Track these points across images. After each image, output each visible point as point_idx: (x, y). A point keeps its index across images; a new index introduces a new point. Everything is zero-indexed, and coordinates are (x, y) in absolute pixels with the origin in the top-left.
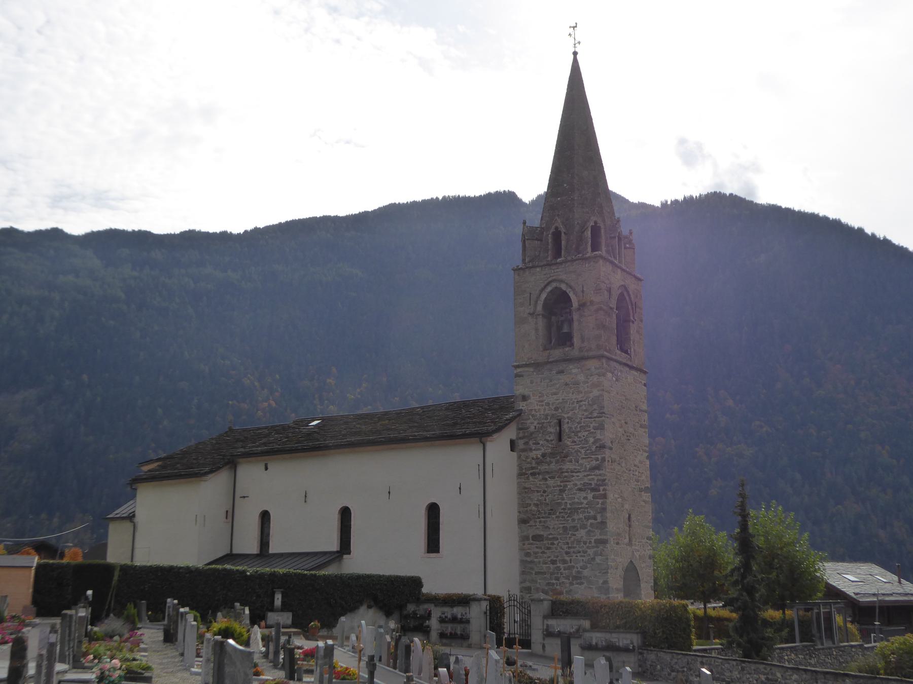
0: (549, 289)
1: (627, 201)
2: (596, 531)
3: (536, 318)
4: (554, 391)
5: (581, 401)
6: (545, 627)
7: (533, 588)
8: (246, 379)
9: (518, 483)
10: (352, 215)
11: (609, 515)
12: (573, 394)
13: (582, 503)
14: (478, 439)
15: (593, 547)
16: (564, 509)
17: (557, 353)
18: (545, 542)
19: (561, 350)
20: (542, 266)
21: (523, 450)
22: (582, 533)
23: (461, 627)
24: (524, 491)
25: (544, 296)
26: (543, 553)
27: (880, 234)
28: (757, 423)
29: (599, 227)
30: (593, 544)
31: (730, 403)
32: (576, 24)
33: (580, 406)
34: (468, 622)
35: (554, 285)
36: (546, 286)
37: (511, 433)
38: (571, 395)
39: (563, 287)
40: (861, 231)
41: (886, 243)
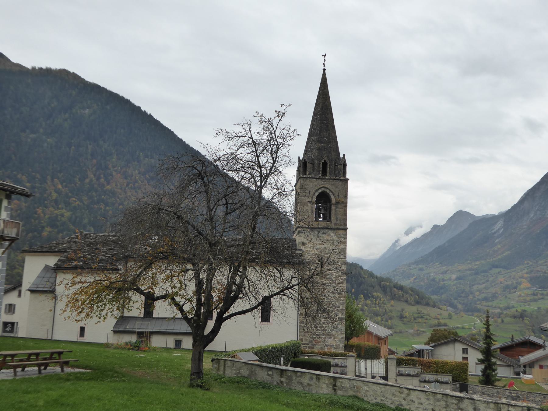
0: (320, 191)
1: (9, 60)
2: (339, 313)
3: (312, 204)
6: (397, 372)
7: (304, 339)
12: (330, 245)
19: (325, 223)
20: (316, 179)
23: (340, 369)
27: (148, 112)
28: (74, 199)
31: (60, 186)
32: (325, 54)
34: (346, 367)
35: (323, 189)
36: (317, 190)
38: (329, 246)
39: (328, 191)
40: (139, 108)
41: (150, 116)
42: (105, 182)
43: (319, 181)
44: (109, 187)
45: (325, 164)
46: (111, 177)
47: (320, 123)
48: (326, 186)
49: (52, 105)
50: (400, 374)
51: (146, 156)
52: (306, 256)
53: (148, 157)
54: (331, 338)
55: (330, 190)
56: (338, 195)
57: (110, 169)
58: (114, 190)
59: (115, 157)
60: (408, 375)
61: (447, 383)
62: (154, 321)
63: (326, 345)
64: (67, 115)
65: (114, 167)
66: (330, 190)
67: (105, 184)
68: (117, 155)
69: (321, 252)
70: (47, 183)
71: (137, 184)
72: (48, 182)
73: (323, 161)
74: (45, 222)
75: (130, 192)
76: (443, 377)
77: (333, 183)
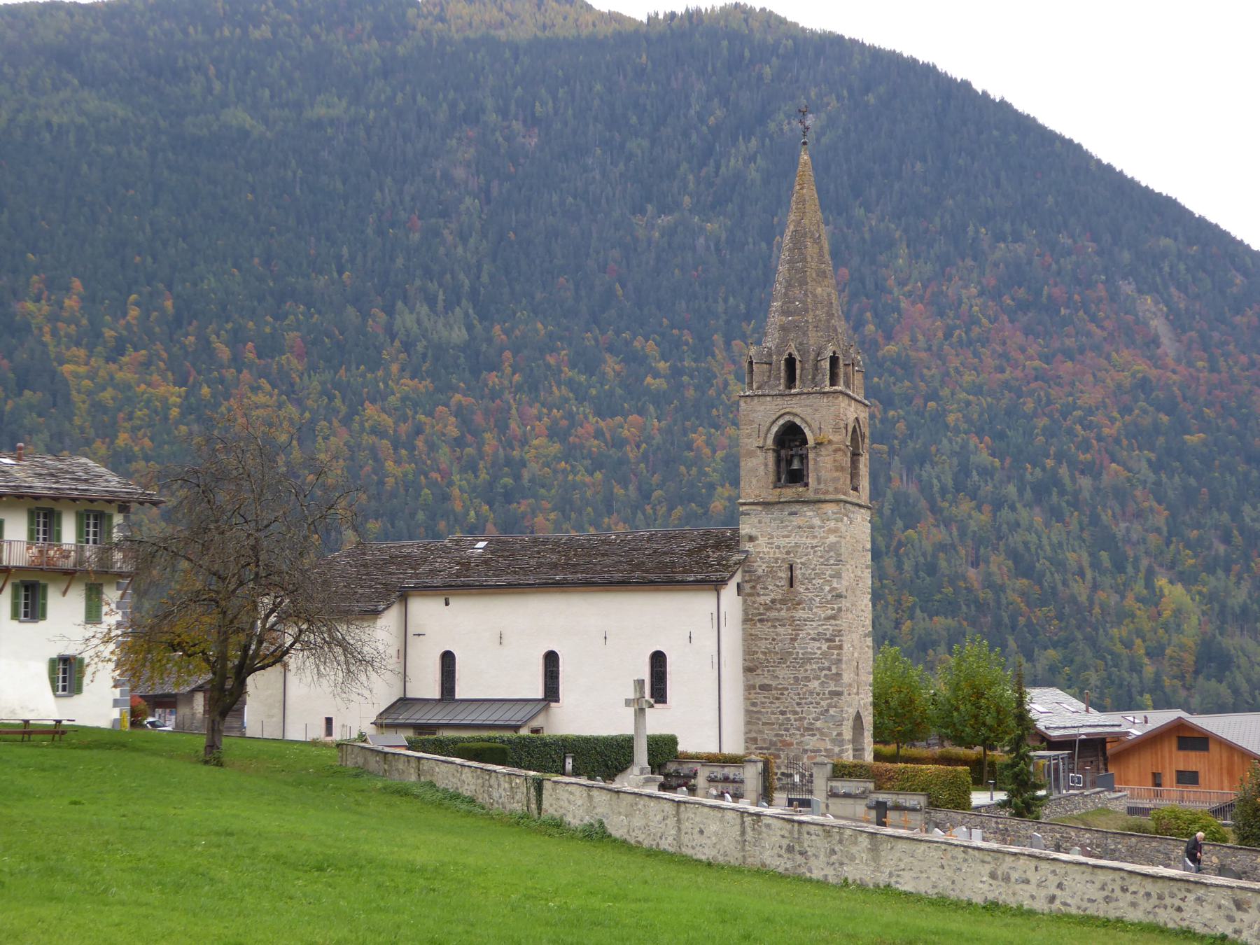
0: (781, 422)
13: (815, 653)
15: (827, 699)
17: (790, 492)
30: (827, 696)
34: (742, 782)
35: (787, 418)
36: (774, 422)
39: (798, 421)
42: (880, 332)
43: (779, 400)
44: (891, 348)
45: (791, 362)
46: (896, 315)
47: (789, 270)
48: (794, 411)
49: (712, 120)
50: (833, 794)
51: (999, 237)
52: (755, 564)
53: (1004, 241)
54: (815, 735)
55: (802, 419)
56: (820, 428)
57: (891, 292)
58: (907, 355)
59: (903, 250)
60: (847, 796)
61: (913, 810)
62: (455, 704)
63: (806, 751)
64: (754, 142)
65: (902, 283)
66: (802, 419)
67: (880, 340)
68: (908, 246)
69: (788, 553)
70: (713, 356)
71: (976, 330)
72: (717, 351)
73: (786, 356)
74: (715, 470)
75: (957, 355)
76: (908, 797)
77: (808, 402)
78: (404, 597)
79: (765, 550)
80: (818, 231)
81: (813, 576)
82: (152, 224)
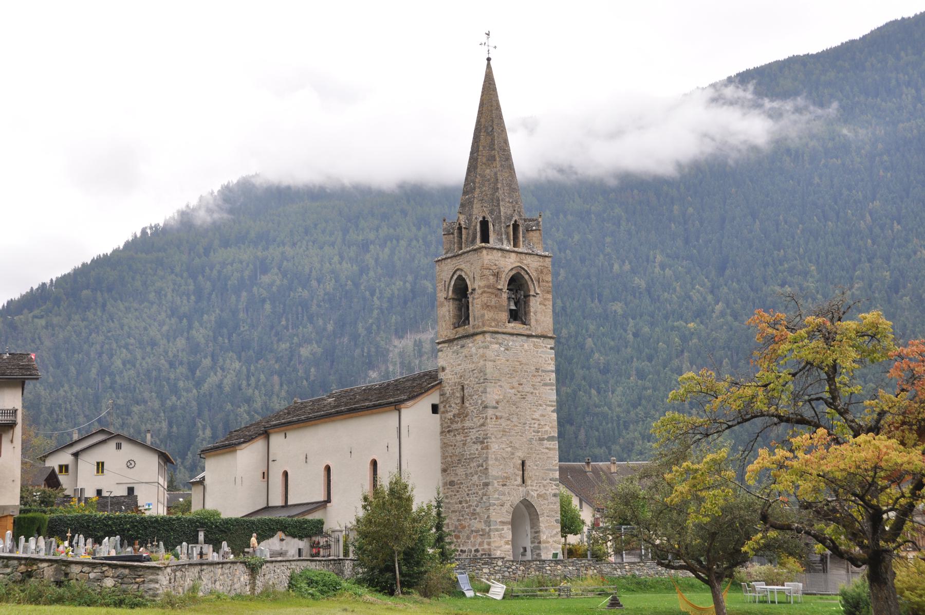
4: (459, 362)
5: (474, 370)
8: (694, 291)
9: (441, 439)
10: (831, 49)
11: (490, 462)
13: (475, 454)
14: (393, 407)
15: (482, 489)
16: (465, 459)
17: (461, 331)
18: (456, 487)
21: (443, 412)
22: (476, 477)
24: (444, 446)
25: (453, 283)
26: (455, 495)
29: (487, 221)
30: (482, 487)
33: (473, 374)
35: (458, 273)
36: (452, 278)
37: (433, 398)
56: (474, 277)
78: (266, 434)
79: (450, 377)
80: (492, 126)
81: (473, 393)
82: (871, 215)
